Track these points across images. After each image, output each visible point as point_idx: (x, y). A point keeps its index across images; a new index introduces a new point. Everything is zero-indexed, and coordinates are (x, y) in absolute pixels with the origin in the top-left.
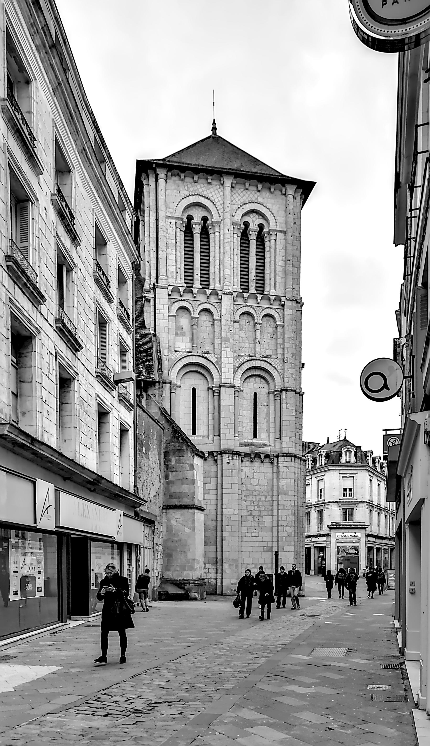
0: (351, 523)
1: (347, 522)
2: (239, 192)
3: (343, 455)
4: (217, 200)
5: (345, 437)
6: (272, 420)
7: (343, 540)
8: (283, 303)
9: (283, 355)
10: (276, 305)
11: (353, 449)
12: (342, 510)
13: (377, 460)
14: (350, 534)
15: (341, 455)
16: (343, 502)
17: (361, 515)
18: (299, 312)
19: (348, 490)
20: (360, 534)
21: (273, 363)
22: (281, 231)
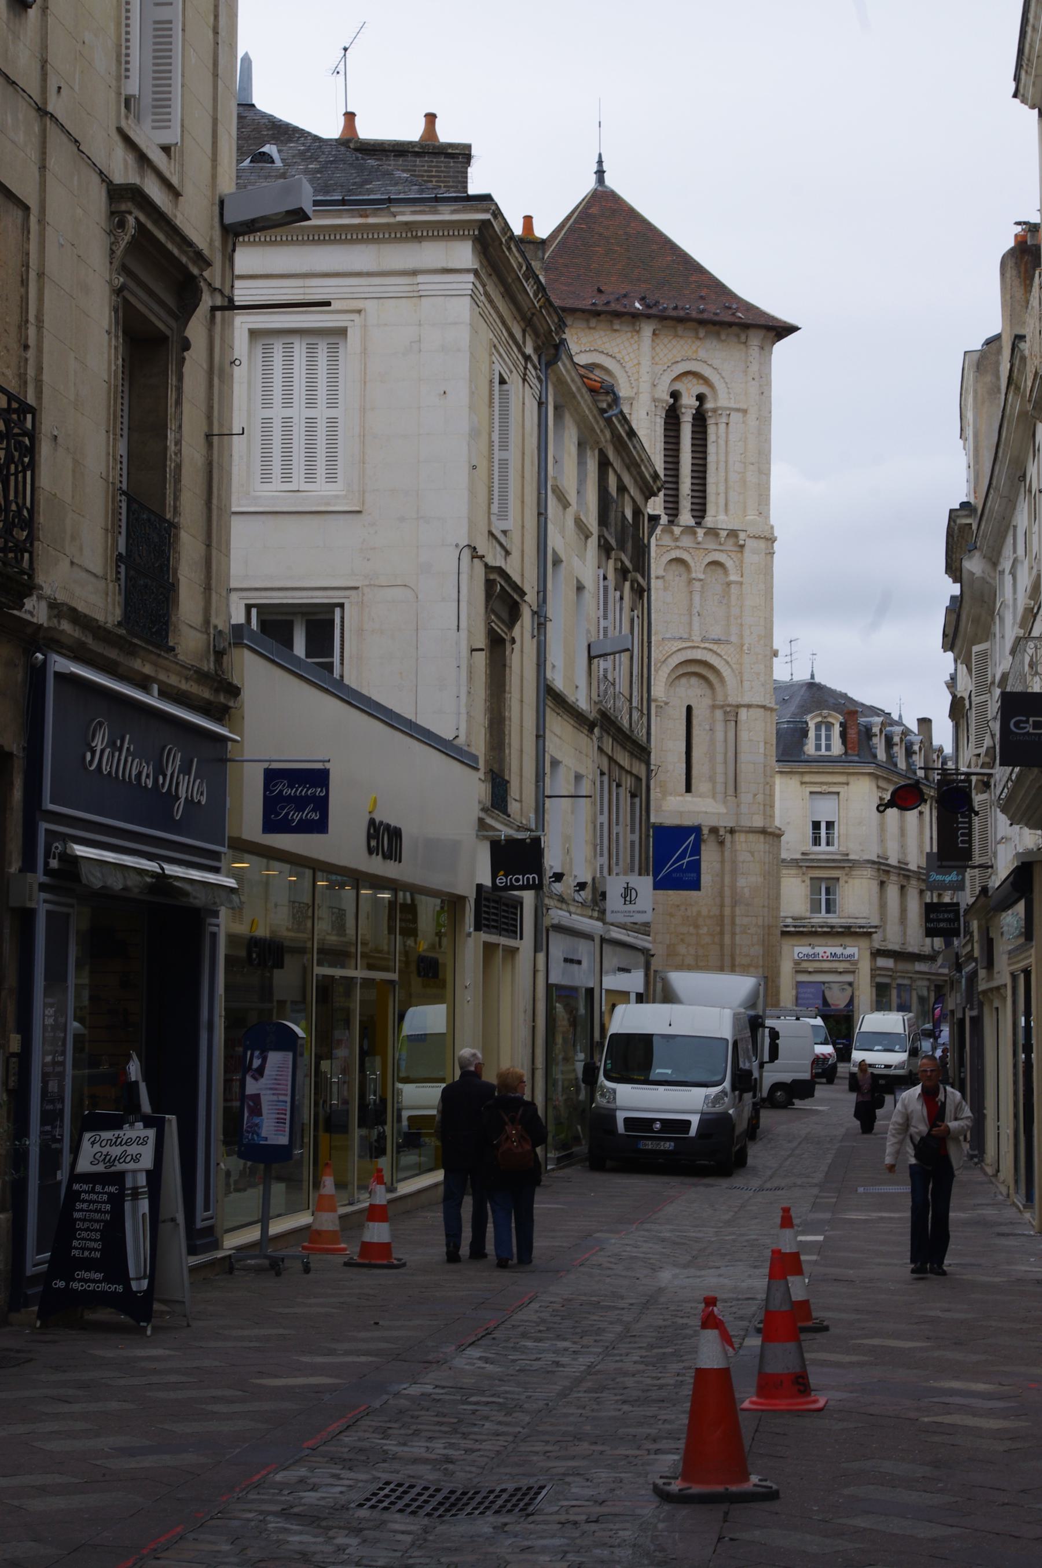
0: (833, 919)
1: (822, 917)
2: (666, 341)
3: (812, 734)
4: (627, 358)
5: (812, 676)
6: (720, 758)
7: (811, 966)
8: (741, 542)
9: (741, 637)
10: (729, 545)
11: (836, 718)
12: (808, 882)
13: (896, 739)
14: (830, 950)
15: (805, 733)
16: (812, 860)
17: (857, 899)
18: (769, 557)
19: (823, 826)
20: (853, 949)
21: (722, 654)
22: (738, 410)
